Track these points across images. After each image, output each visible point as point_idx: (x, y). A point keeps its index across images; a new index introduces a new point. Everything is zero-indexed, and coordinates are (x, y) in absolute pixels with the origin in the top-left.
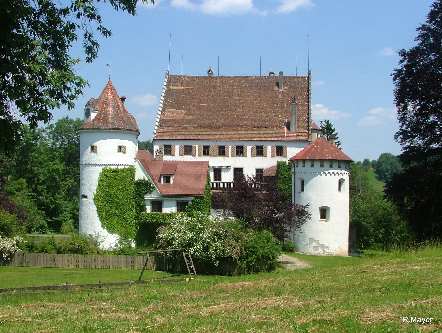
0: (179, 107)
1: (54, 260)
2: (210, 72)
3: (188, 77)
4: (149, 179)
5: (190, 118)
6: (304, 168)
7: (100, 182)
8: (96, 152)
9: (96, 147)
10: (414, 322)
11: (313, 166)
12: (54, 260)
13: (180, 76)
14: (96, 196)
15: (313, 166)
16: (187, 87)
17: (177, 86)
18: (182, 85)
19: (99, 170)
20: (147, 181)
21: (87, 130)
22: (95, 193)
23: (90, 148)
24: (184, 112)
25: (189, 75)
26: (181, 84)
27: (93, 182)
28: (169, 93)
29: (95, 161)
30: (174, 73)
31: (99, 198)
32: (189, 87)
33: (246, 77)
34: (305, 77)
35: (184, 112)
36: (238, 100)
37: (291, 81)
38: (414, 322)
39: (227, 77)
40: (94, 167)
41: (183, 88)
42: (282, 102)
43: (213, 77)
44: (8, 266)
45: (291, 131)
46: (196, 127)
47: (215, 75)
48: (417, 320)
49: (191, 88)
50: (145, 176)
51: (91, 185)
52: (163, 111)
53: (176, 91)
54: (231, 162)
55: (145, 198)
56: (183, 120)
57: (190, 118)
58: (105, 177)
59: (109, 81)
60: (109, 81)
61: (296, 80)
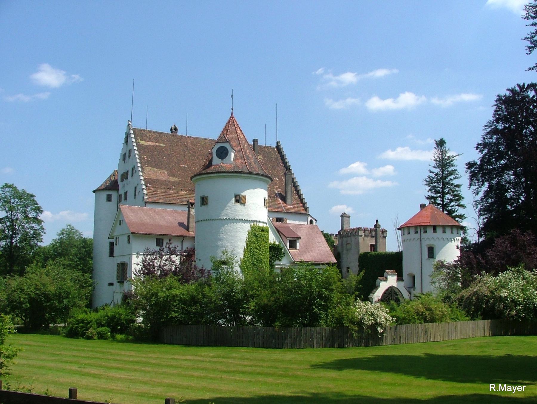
0: (158, 166)
1: (426, 332)
3: (154, 132)
4: (280, 242)
5: (175, 179)
6: (435, 234)
7: (249, 242)
8: (244, 204)
9: (245, 197)
10: (503, 390)
11: (444, 232)
12: (426, 332)
13: (144, 131)
14: (244, 261)
15: (444, 232)
16: (157, 144)
17: (145, 140)
18: (150, 140)
19: (247, 227)
20: (279, 246)
21: (242, 175)
22: (242, 257)
23: (234, 200)
25: (224, 127)
26: (150, 139)
27: (239, 243)
29: (242, 215)
30: (139, 124)
31: (248, 264)
32: (160, 144)
34: (273, 148)
38: (503, 390)
39: (197, 138)
40: (241, 225)
41: (153, 144)
44: (379, 345)
45: (287, 203)
46: (187, 190)
48: (507, 388)
49: (162, 145)
50: (275, 238)
51: (235, 247)
55: (276, 267)
57: (175, 179)
58: (254, 238)
59: (232, 117)
60: (232, 117)
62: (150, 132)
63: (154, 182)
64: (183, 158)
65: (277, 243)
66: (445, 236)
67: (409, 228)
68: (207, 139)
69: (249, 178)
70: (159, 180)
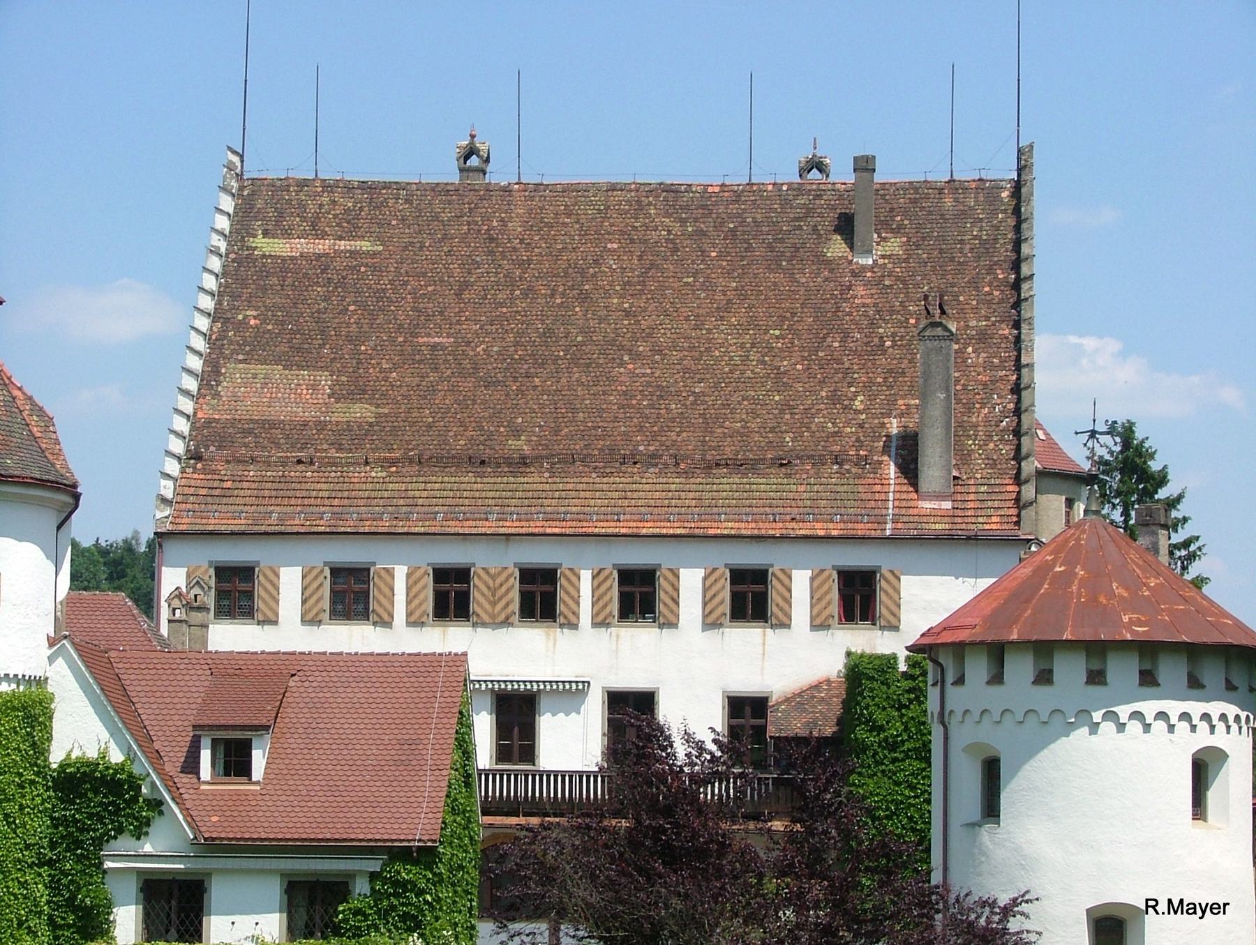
0: (297, 356)
2: (474, 161)
4: (131, 757)
5: (361, 411)
6: (1043, 690)
11: (1044, 677)
13: (302, 184)
15: (1044, 677)
17: (287, 234)
20: (121, 768)
24: (325, 380)
28: (243, 275)
30: (274, 161)
33: (671, 190)
35: (325, 380)
36: (627, 314)
37: (916, 207)
39: (568, 189)
41: (322, 246)
42: (873, 324)
43: (488, 188)
45: (924, 486)
46: (393, 463)
47: (499, 175)
50: (105, 735)
52: (210, 378)
53: (284, 265)
54: (585, 656)
56: (321, 426)
57: (361, 411)
61: (948, 201)
62: (328, 187)
63: (250, 432)
64: (451, 299)
65: (116, 757)
66: (1044, 698)
67: (959, 649)
68: (622, 188)
69: (23, 500)
70: (273, 425)
